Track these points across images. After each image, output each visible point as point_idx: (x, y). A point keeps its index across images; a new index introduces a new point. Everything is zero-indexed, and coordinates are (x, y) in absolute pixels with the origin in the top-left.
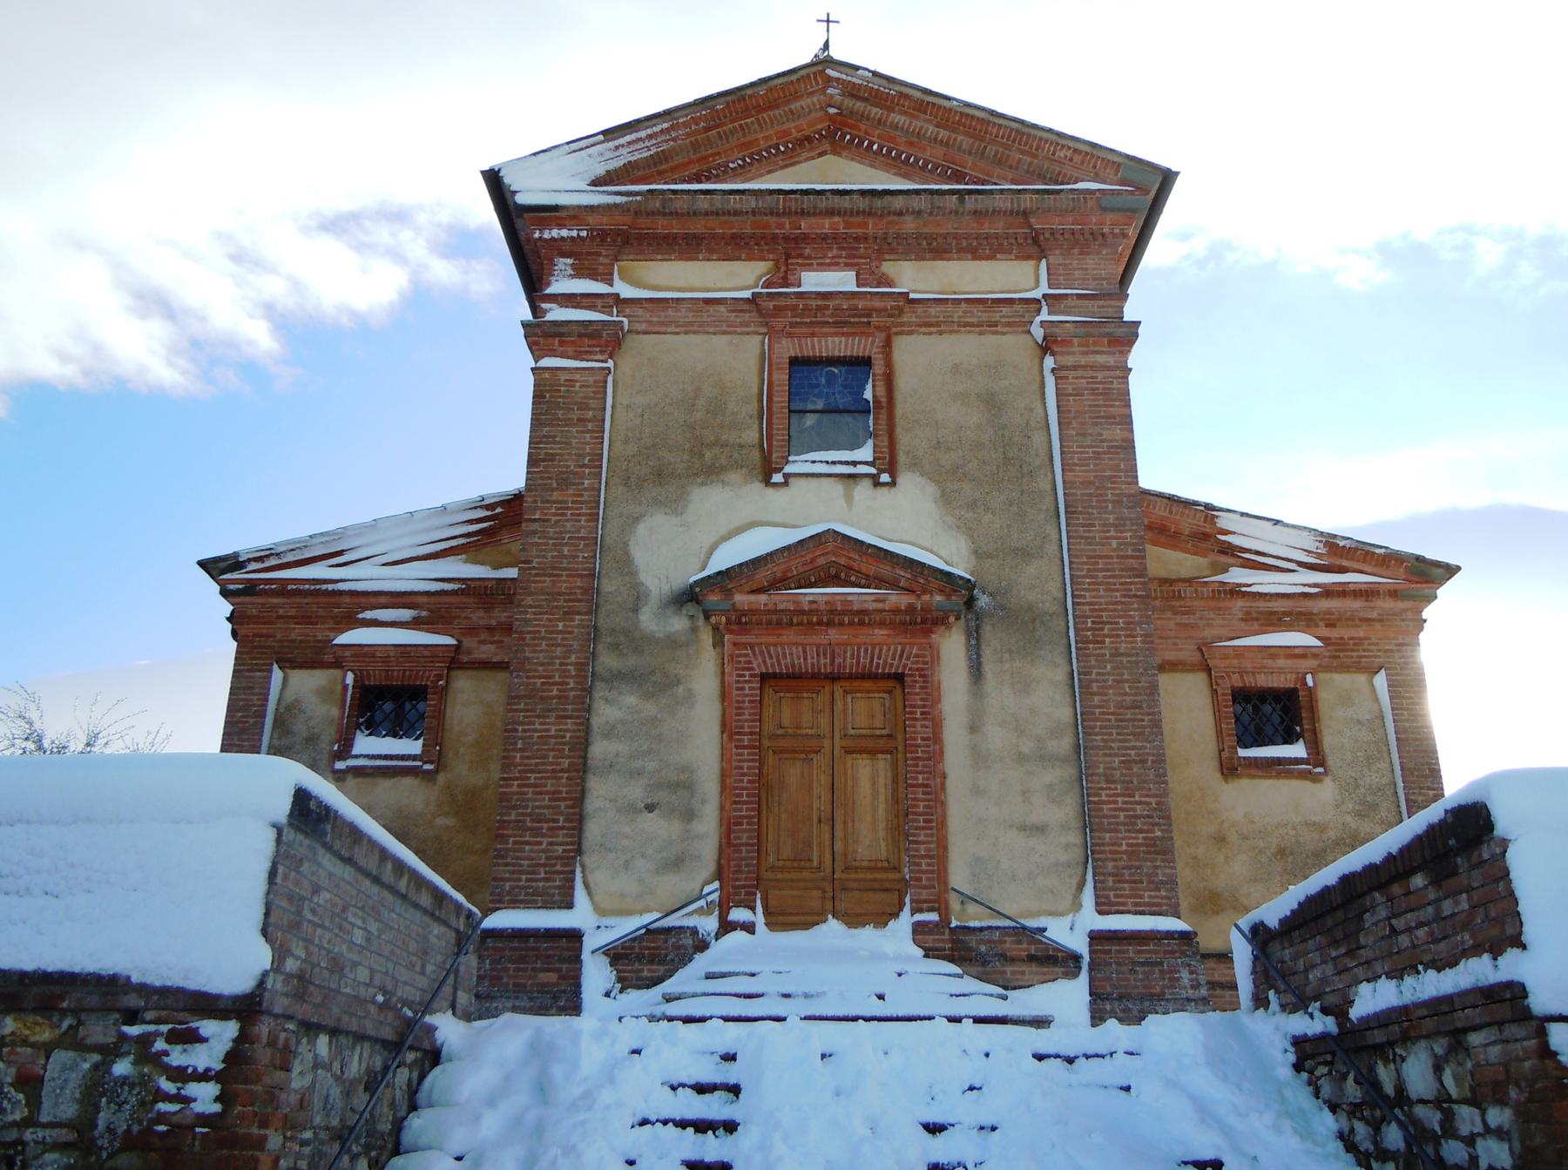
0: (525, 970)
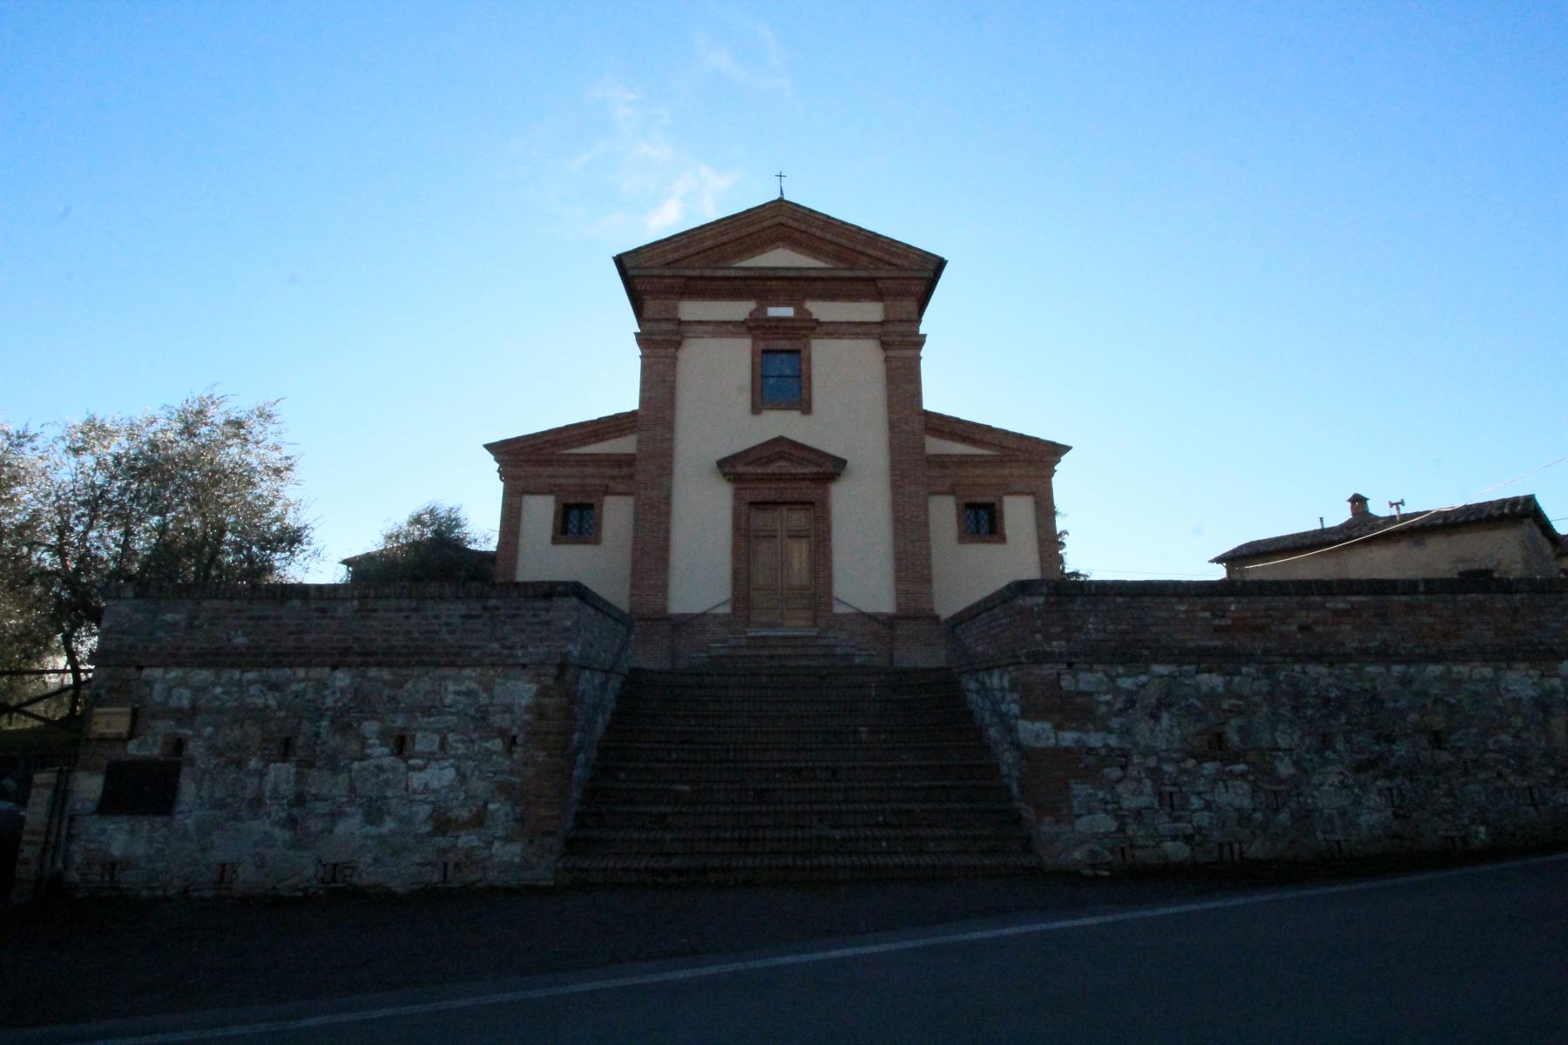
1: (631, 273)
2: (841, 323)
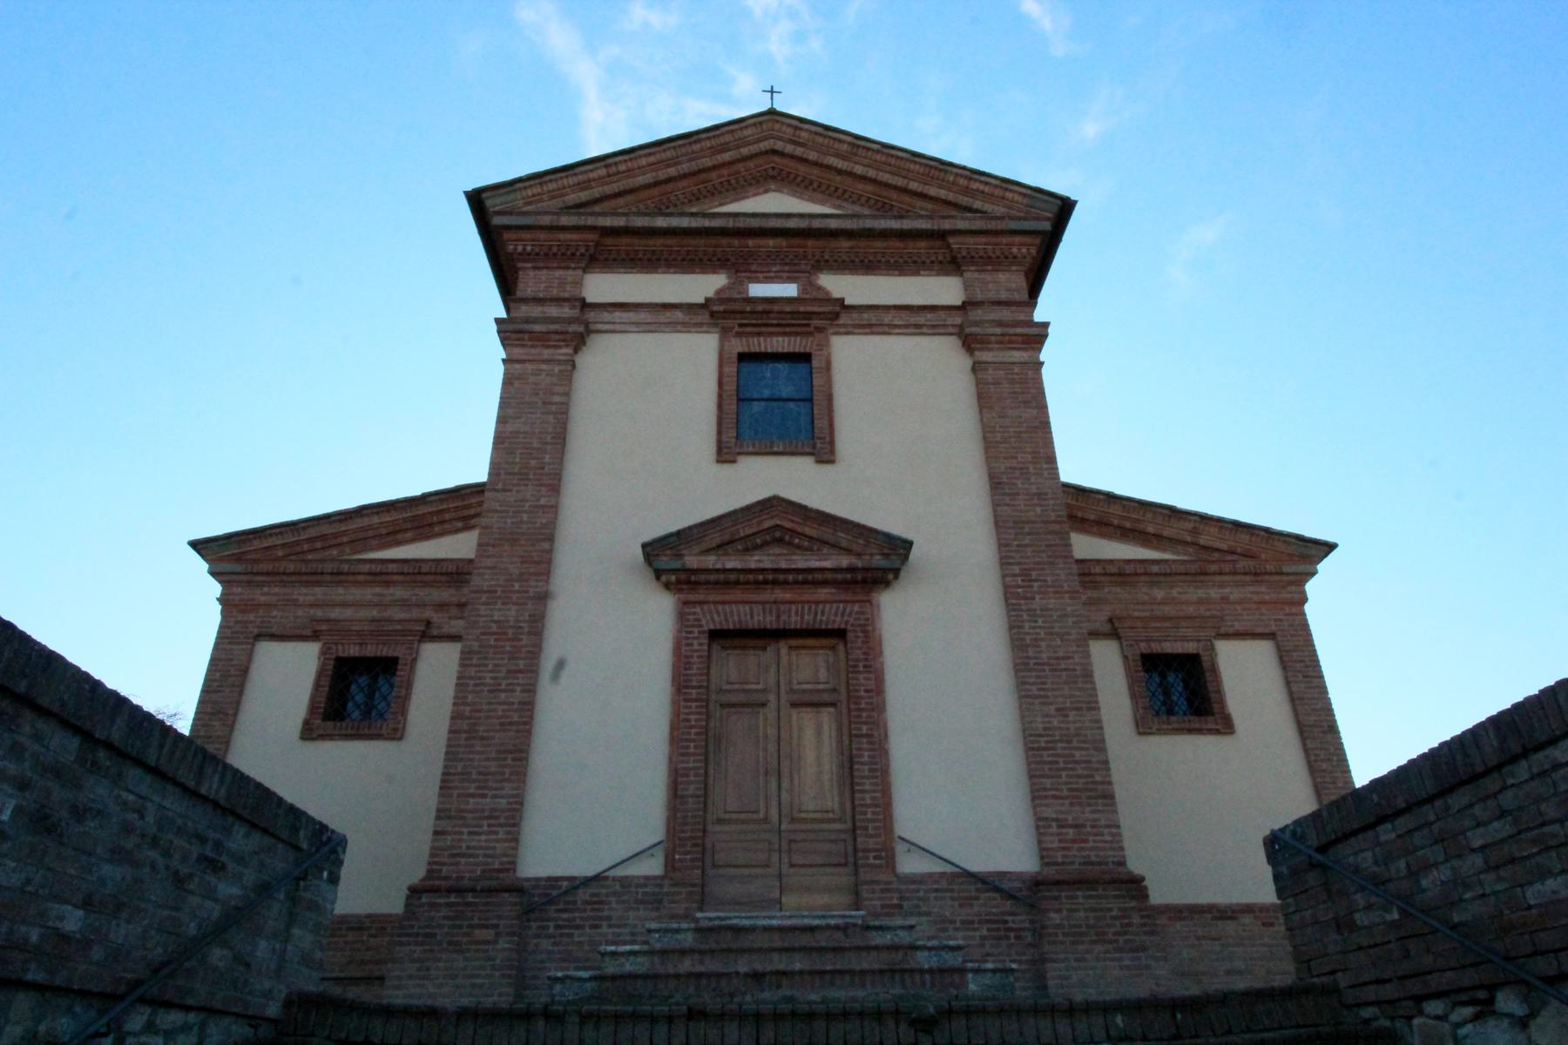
0: (460, 927)
1: (497, 221)
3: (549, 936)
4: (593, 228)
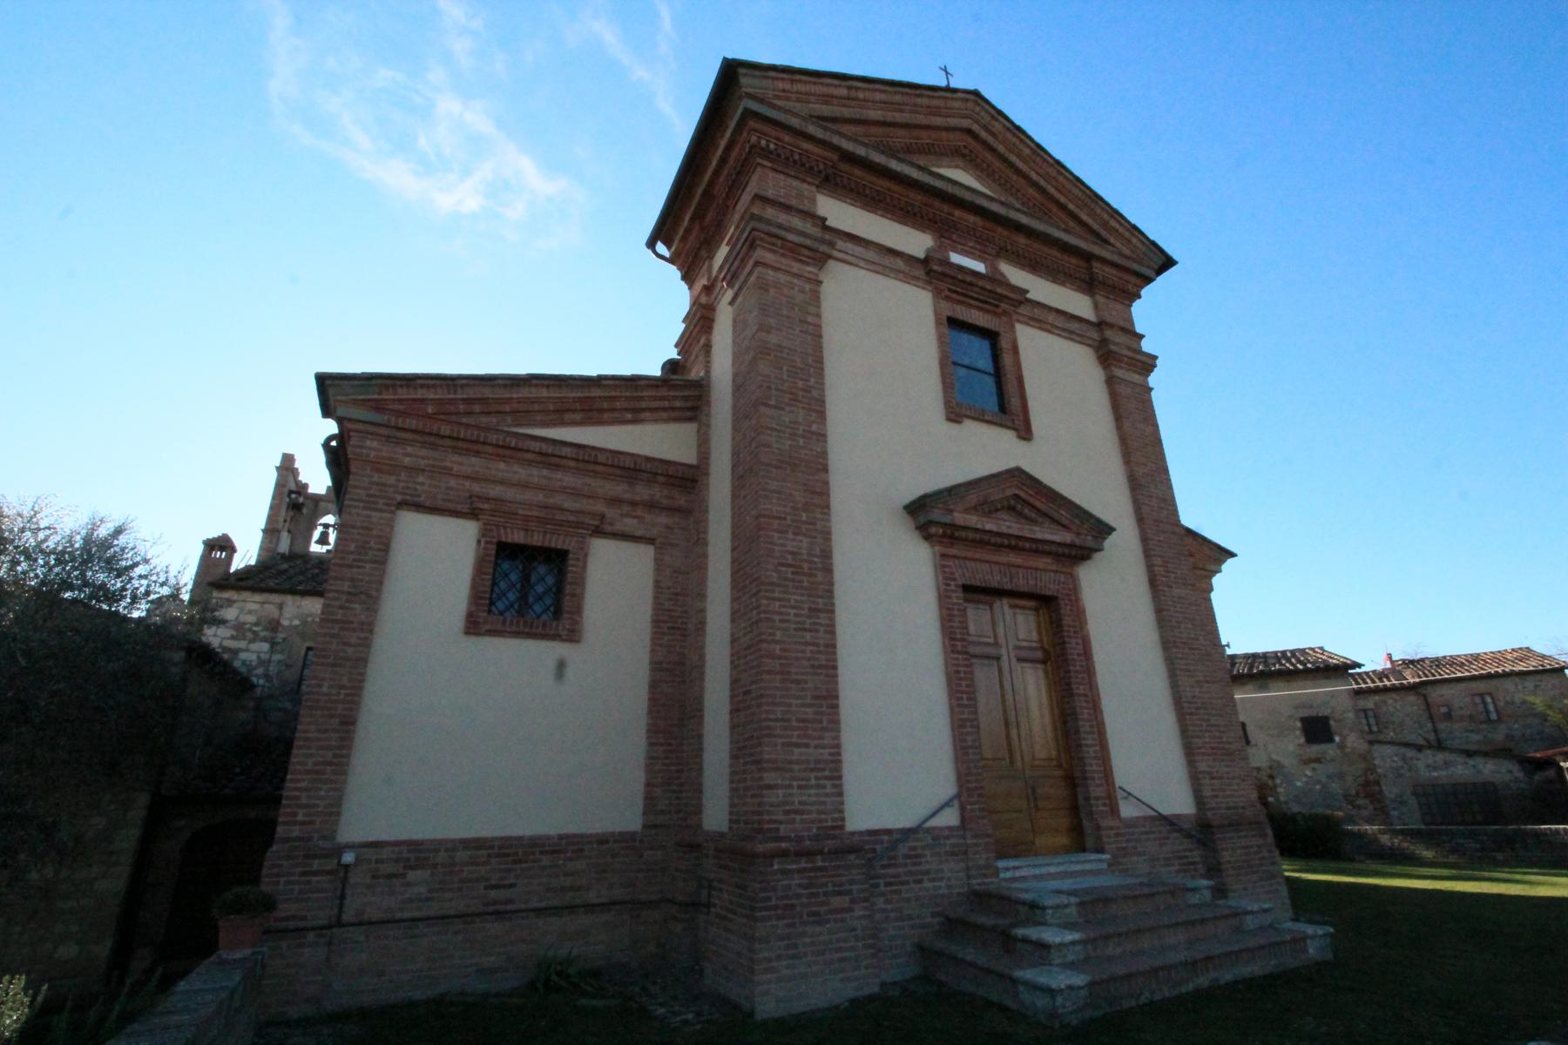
0: (816, 895)
2: (1050, 309)
3: (883, 894)
4: (836, 149)
